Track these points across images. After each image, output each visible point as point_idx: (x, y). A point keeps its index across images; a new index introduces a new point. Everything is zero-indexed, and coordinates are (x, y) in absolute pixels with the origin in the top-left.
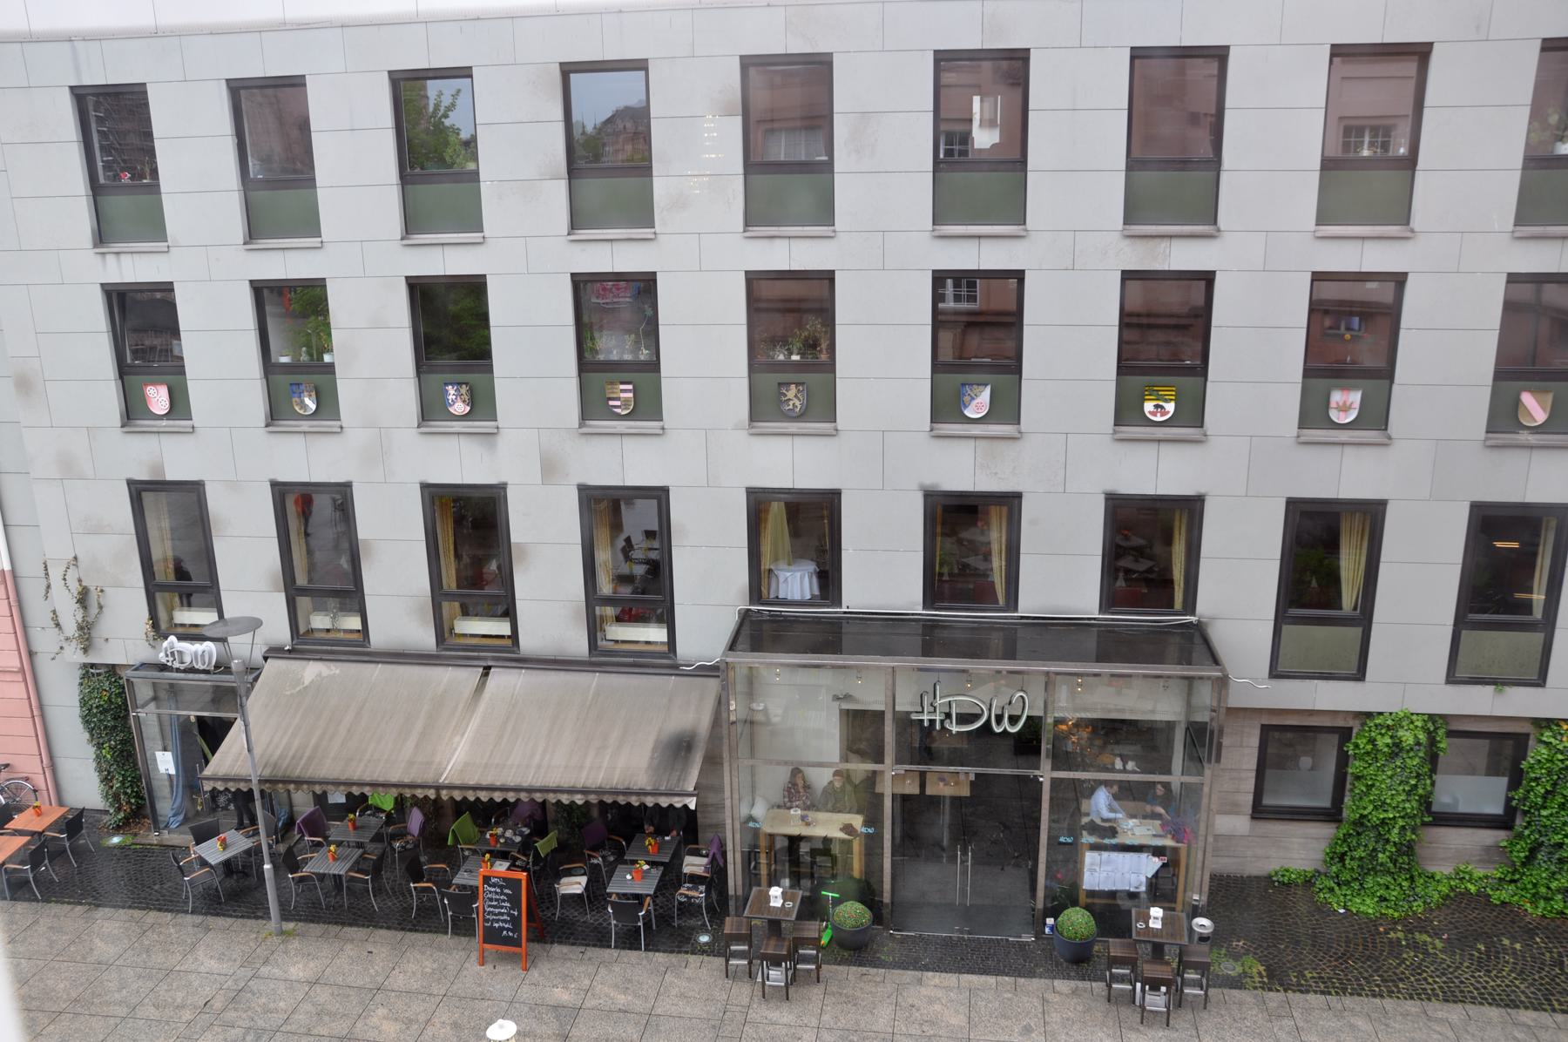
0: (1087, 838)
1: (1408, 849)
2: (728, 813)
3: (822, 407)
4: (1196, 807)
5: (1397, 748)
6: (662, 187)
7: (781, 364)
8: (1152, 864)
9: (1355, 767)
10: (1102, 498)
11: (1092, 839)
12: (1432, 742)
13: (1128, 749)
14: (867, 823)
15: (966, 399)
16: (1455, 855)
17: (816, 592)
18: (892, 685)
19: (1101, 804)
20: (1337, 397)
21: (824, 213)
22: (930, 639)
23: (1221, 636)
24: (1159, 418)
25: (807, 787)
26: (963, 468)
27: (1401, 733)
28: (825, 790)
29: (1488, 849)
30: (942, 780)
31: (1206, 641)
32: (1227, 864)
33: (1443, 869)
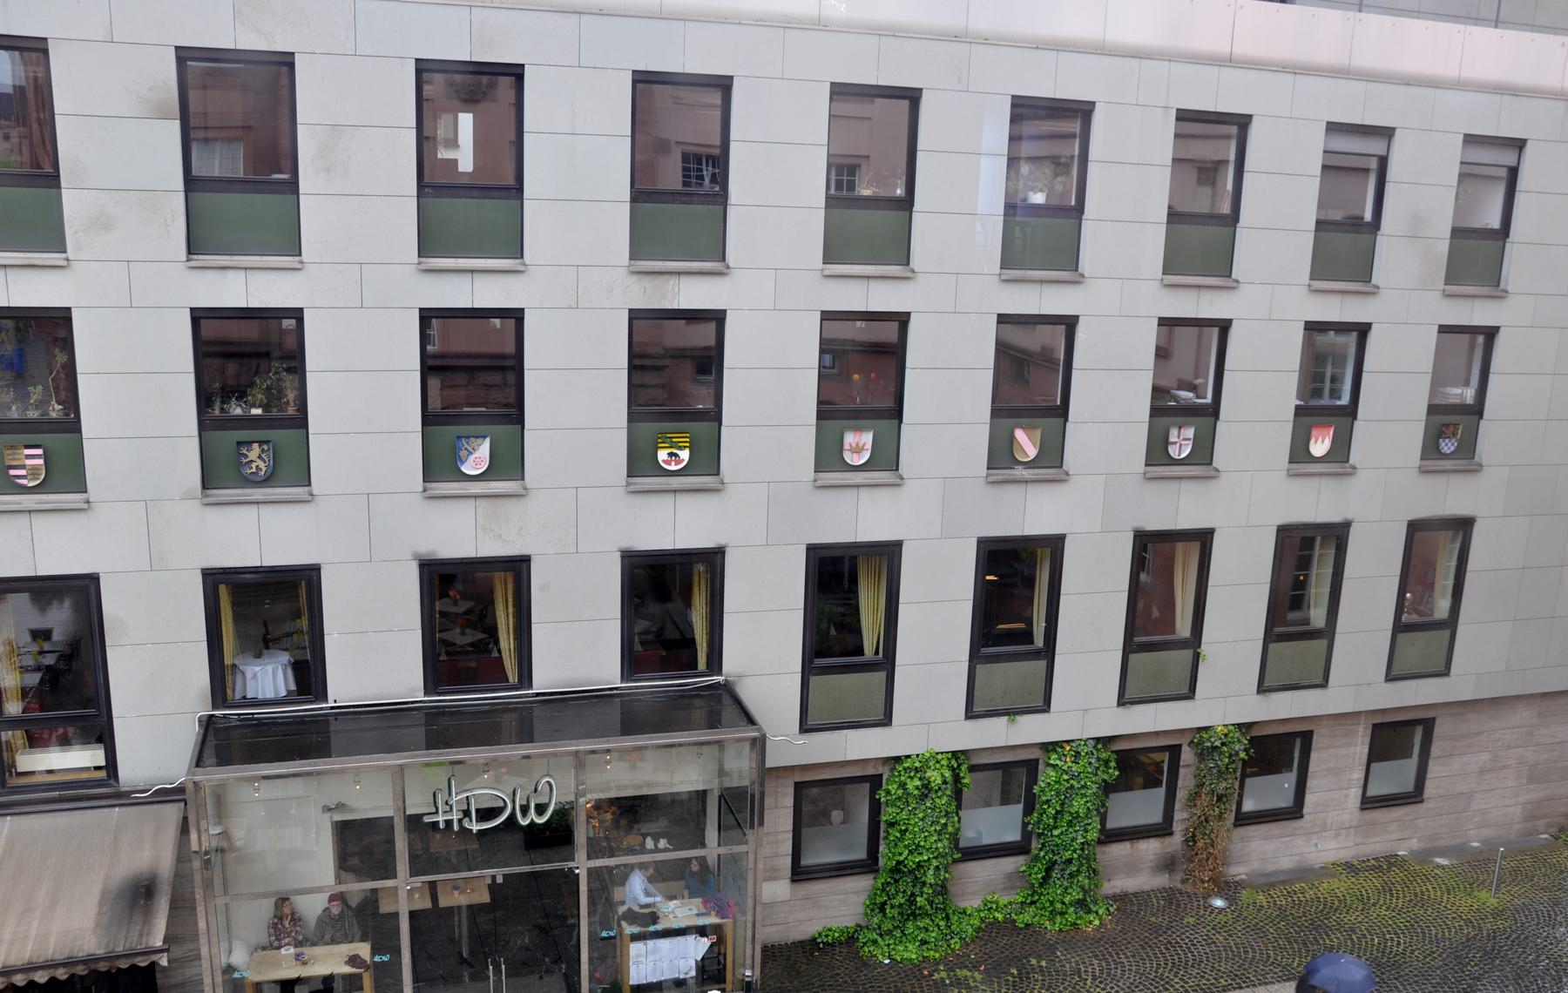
0: (629, 929)
1: (942, 889)
2: (205, 964)
3: (292, 469)
4: (740, 877)
5: (926, 788)
6: (74, 203)
7: (238, 419)
8: (697, 947)
9: (887, 814)
10: (618, 555)
11: (636, 930)
12: (957, 779)
13: (654, 827)
14: (375, 951)
15: (463, 453)
16: (983, 887)
17: (293, 687)
18: (369, 787)
19: (637, 890)
20: (850, 438)
21: (512, 244)
22: (439, 729)
23: (750, 693)
24: (673, 467)
25: (296, 919)
26: (464, 531)
27: (929, 774)
28: (320, 920)
29: (1010, 876)
30: (456, 888)
31: (738, 702)
32: (772, 933)
33: (972, 903)
